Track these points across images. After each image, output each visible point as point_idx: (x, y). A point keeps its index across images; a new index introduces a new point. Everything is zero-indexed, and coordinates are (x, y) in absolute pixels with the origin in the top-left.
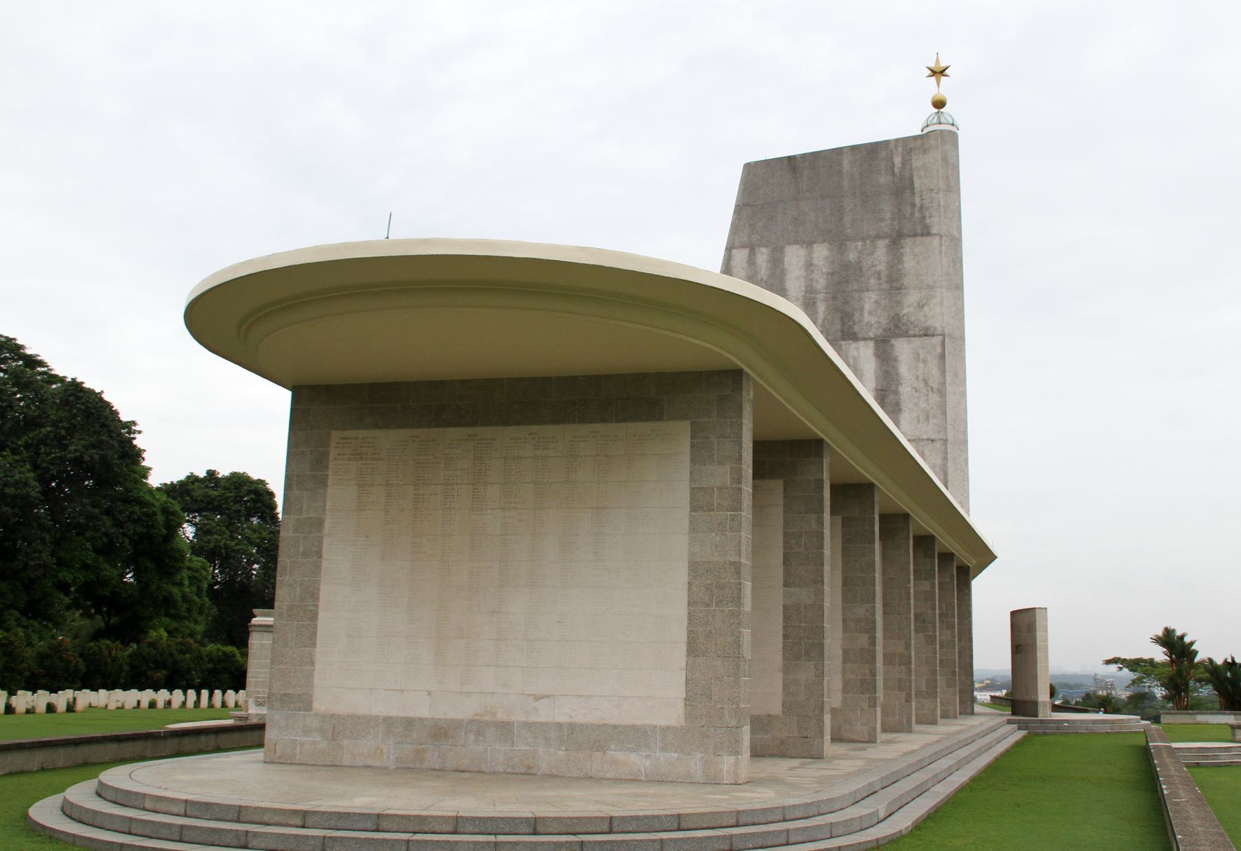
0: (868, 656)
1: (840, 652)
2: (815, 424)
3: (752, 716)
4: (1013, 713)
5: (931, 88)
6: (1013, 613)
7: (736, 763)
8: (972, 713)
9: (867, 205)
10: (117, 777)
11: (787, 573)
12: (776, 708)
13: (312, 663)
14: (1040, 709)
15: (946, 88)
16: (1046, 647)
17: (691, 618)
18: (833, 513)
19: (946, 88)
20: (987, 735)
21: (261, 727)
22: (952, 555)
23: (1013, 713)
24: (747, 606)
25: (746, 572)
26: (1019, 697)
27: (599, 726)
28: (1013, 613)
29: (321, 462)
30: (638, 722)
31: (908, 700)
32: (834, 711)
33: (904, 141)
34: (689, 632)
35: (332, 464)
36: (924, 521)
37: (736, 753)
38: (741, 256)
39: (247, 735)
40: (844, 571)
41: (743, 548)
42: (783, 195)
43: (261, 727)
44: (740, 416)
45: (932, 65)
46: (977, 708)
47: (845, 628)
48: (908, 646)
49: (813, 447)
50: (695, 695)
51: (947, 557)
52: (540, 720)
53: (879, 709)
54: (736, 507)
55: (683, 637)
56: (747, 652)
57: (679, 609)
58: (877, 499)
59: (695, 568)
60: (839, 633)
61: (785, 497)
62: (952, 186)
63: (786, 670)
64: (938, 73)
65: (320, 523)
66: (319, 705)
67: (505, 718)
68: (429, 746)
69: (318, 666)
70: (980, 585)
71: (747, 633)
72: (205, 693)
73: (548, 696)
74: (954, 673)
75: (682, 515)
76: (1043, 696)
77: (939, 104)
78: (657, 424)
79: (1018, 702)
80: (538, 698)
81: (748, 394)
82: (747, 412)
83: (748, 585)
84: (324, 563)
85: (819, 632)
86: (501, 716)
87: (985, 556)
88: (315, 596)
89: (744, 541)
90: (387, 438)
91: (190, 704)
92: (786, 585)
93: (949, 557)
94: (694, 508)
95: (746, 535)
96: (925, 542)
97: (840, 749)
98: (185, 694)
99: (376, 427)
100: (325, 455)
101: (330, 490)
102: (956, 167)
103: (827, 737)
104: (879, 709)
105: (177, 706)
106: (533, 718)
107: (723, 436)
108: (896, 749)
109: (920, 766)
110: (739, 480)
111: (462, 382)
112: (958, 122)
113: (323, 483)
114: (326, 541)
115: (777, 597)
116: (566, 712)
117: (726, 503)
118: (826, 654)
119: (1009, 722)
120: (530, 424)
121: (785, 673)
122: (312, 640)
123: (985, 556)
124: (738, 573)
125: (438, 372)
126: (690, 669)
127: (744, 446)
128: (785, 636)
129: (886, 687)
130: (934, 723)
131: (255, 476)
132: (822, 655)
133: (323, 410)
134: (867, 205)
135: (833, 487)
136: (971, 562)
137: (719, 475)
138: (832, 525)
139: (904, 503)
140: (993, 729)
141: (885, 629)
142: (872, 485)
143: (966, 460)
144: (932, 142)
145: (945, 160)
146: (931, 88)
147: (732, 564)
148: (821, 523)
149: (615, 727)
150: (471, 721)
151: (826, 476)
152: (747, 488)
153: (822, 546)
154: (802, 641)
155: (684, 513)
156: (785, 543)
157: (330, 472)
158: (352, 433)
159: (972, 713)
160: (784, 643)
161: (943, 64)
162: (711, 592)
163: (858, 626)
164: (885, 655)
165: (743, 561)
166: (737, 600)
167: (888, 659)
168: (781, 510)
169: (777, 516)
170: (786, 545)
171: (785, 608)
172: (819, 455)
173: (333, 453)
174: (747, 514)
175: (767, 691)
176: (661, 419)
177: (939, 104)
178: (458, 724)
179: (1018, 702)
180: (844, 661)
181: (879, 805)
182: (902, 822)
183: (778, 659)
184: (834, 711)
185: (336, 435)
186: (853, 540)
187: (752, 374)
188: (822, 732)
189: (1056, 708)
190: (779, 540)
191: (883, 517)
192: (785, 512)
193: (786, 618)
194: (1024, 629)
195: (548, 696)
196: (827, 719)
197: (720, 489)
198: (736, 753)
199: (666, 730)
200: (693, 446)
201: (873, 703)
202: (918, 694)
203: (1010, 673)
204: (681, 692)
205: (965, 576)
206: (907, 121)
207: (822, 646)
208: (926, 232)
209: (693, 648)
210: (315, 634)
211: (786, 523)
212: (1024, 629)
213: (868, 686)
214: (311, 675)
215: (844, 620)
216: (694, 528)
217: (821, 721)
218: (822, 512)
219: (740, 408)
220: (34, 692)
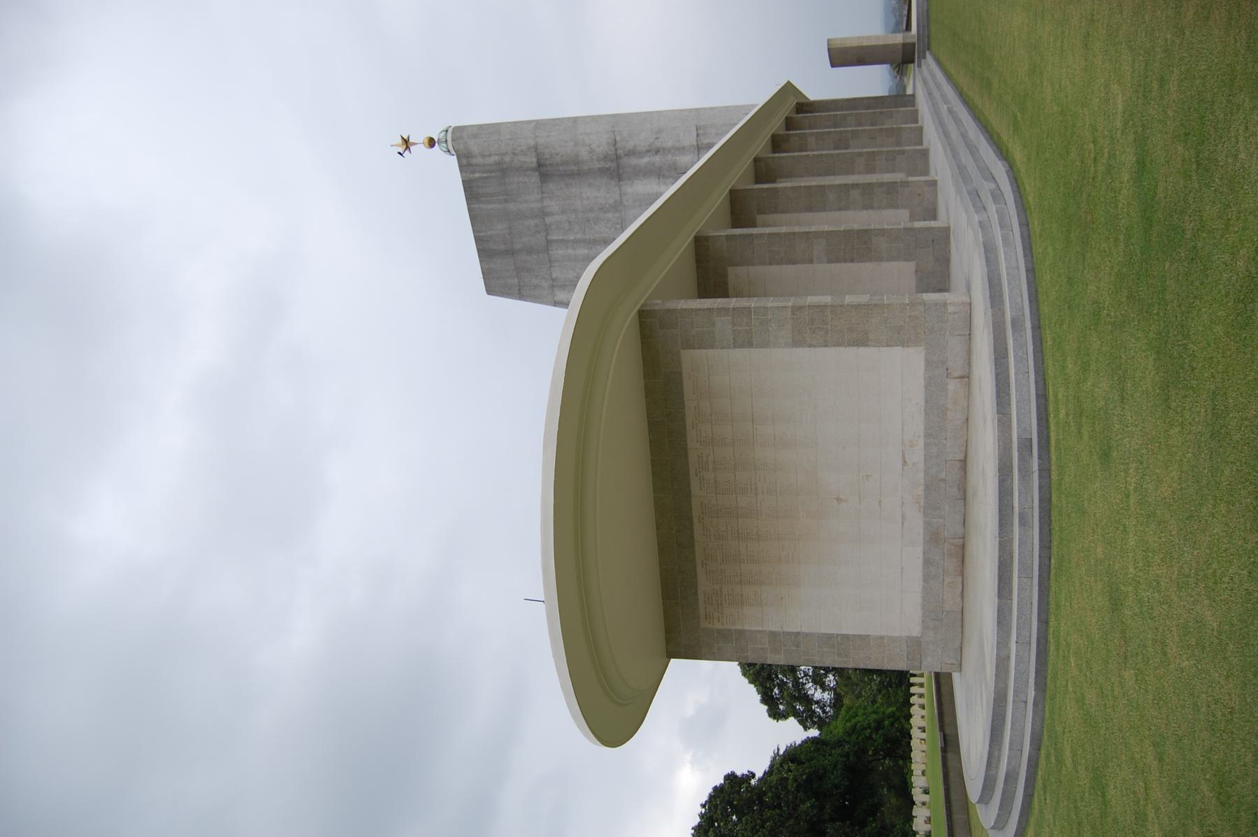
0: (868, 188)
2: (682, 244)
3: (918, 292)
4: (913, 62)
5: (419, 150)
6: (833, 65)
7: (952, 304)
8: (913, 96)
9: (517, 194)
10: (974, 789)
11: (803, 261)
12: (910, 267)
13: (882, 638)
14: (908, 41)
15: (418, 137)
16: (859, 38)
17: (839, 345)
18: (754, 225)
19: (418, 137)
20: (928, 84)
21: (937, 675)
22: (787, 118)
23: (913, 62)
24: (827, 299)
25: (800, 301)
26: (899, 58)
27: (926, 414)
28: (833, 65)
29: (725, 635)
30: (922, 382)
31: (903, 152)
32: (913, 218)
33: (462, 168)
34: (849, 345)
35: (727, 627)
36: (760, 145)
37: (945, 304)
38: (561, 296)
39: (943, 684)
40: (799, 211)
41: (780, 304)
42: (510, 260)
43: (937, 675)
44: (675, 310)
46: (909, 91)
47: (846, 208)
48: (860, 154)
49: (701, 244)
50: (899, 338)
51: (789, 124)
53: (910, 179)
54: (747, 311)
55: (852, 350)
56: (864, 299)
57: (831, 353)
58: (741, 187)
59: (797, 343)
60: (849, 214)
62: (494, 129)
63: (880, 259)
64: (407, 143)
65: (773, 635)
66: (916, 631)
67: (922, 488)
68: (948, 551)
69: (884, 633)
70: (813, 95)
71: (849, 299)
72: (912, 680)
74: (881, 113)
75: (754, 355)
76: (899, 38)
77: (432, 143)
78: (685, 375)
79: (903, 59)
80: (905, 463)
81: (658, 304)
82: (672, 305)
83: (812, 300)
84: (805, 630)
85: (848, 234)
86: (920, 491)
87: (788, 89)
88: (829, 637)
89: (775, 304)
90: (704, 585)
91: (922, 701)
92: (811, 261)
93: (792, 123)
94: (750, 345)
95: (770, 303)
96: (777, 143)
97: (942, 213)
98: (912, 685)
99: (696, 593)
100: (719, 631)
101: (747, 627)
102: (481, 127)
103: (933, 224)
104: (910, 179)
105: (921, 718)
106: (921, 466)
108: (941, 166)
109: (955, 155)
110: (725, 311)
111: (658, 528)
112: (445, 127)
113: (741, 633)
114: (786, 629)
115: (823, 269)
116: (917, 426)
118: (865, 228)
119: (919, 66)
120: (688, 475)
122: (864, 638)
123: (789, 89)
124: (801, 308)
125: (655, 546)
126: (878, 344)
127: (699, 306)
128: (852, 261)
129: (893, 171)
130: (921, 129)
131: (710, 790)
132: (866, 231)
133: (685, 635)
134: (517, 194)
135: (734, 226)
136: (792, 102)
137: (723, 326)
138: (764, 225)
139: (746, 163)
140: (925, 82)
141: (847, 173)
142: (731, 191)
143: (712, 109)
144: (462, 147)
145: (475, 136)
146: (419, 150)
147: (793, 314)
148: (761, 235)
149: (927, 402)
150: (925, 514)
151: (723, 233)
152: (733, 302)
153: (779, 235)
154: (855, 247)
155: (755, 354)
156: (777, 263)
157: (733, 628)
158: (702, 612)
159: (913, 96)
161: (400, 141)
162: (818, 328)
163: (844, 198)
164: (868, 172)
165: (790, 304)
166: (822, 308)
167: (870, 170)
168: (751, 268)
169: (757, 271)
170: (780, 262)
171: (830, 261)
172: (707, 239)
173: (718, 626)
174: (753, 303)
175: (897, 275)
176: (680, 373)
177: (432, 143)
178: (927, 524)
179: (903, 59)
180: (872, 208)
181: (986, 188)
182: (999, 169)
183: (869, 266)
184: (913, 218)
185: (704, 624)
186: (772, 205)
187: (642, 302)
188: (928, 229)
189: (908, 28)
190: (775, 269)
191: (758, 181)
192: (753, 264)
193: (838, 261)
194: (842, 56)
196: (918, 225)
198: (945, 304)
199: (929, 363)
200: (700, 348)
201: (905, 184)
202: (899, 144)
203: (884, 66)
204: (898, 350)
205: (804, 107)
206: (447, 168)
207: (859, 231)
208: (536, 148)
209: (862, 342)
210: (860, 636)
211: (762, 263)
212: (842, 56)
213: (892, 188)
214: (892, 639)
215: (840, 209)
216: (765, 344)
217: (920, 230)
218: (751, 235)
219: (668, 310)
220: (914, 803)
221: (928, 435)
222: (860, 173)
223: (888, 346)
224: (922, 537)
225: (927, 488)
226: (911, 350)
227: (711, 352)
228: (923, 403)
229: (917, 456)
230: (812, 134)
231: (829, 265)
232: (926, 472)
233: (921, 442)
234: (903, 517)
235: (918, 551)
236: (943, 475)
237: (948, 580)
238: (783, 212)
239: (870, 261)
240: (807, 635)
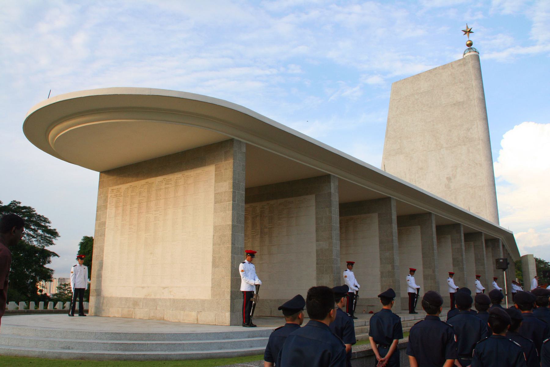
1: (379, 273)
5: (466, 39)
45: (465, 29)
47: (381, 263)
52: (165, 298)
59: (215, 228)
61: (316, 202)
67: (154, 297)
73: (167, 288)
80: (164, 288)
84: (106, 239)
86: (153, 297)
92: (317, 241)
94: (216, 203)
100: (107, 197)
107: (226, 169)
117: (227, 198)
121: (317, 280)
126: (213, 274)
128: (317, 264)
146: (466, 39)
149: (188, 300)
150: (144, 299)
155: (211, 205)
160: (317, 267)
161: (470, 28)
168: (314, 208)
170: (317, 223)
171: (317, 251)
177: (470, 45)
180: (381, 277)
183: (314, 274)
192: (316, 208)
193: (318, 256)
195: (167, 288)
197: (225, 192)
199: (203, 301)
211: (317, 213)
215: (381, 259)
221: (174, 301)
222: (424, 272)
223: (212, 279)
224: (136, 297)
225: (154, 300)
226: (210, 292)
227: (213, 181)
228: (187, 298)
229: (166, 295)
230: (461, 245)
231: (315, 251)
232: (160, 299)
233: (172, 297)
234: (143, 287)
235: (130, 295)
236: (158, 308)
237: (120, 309)
238: (380, 227)
239: (317, 274)
240: (104, 240)
